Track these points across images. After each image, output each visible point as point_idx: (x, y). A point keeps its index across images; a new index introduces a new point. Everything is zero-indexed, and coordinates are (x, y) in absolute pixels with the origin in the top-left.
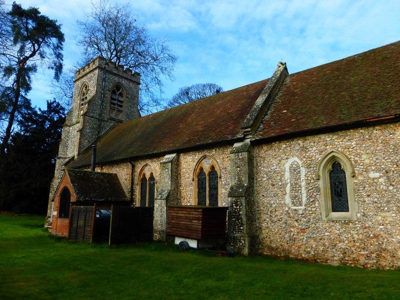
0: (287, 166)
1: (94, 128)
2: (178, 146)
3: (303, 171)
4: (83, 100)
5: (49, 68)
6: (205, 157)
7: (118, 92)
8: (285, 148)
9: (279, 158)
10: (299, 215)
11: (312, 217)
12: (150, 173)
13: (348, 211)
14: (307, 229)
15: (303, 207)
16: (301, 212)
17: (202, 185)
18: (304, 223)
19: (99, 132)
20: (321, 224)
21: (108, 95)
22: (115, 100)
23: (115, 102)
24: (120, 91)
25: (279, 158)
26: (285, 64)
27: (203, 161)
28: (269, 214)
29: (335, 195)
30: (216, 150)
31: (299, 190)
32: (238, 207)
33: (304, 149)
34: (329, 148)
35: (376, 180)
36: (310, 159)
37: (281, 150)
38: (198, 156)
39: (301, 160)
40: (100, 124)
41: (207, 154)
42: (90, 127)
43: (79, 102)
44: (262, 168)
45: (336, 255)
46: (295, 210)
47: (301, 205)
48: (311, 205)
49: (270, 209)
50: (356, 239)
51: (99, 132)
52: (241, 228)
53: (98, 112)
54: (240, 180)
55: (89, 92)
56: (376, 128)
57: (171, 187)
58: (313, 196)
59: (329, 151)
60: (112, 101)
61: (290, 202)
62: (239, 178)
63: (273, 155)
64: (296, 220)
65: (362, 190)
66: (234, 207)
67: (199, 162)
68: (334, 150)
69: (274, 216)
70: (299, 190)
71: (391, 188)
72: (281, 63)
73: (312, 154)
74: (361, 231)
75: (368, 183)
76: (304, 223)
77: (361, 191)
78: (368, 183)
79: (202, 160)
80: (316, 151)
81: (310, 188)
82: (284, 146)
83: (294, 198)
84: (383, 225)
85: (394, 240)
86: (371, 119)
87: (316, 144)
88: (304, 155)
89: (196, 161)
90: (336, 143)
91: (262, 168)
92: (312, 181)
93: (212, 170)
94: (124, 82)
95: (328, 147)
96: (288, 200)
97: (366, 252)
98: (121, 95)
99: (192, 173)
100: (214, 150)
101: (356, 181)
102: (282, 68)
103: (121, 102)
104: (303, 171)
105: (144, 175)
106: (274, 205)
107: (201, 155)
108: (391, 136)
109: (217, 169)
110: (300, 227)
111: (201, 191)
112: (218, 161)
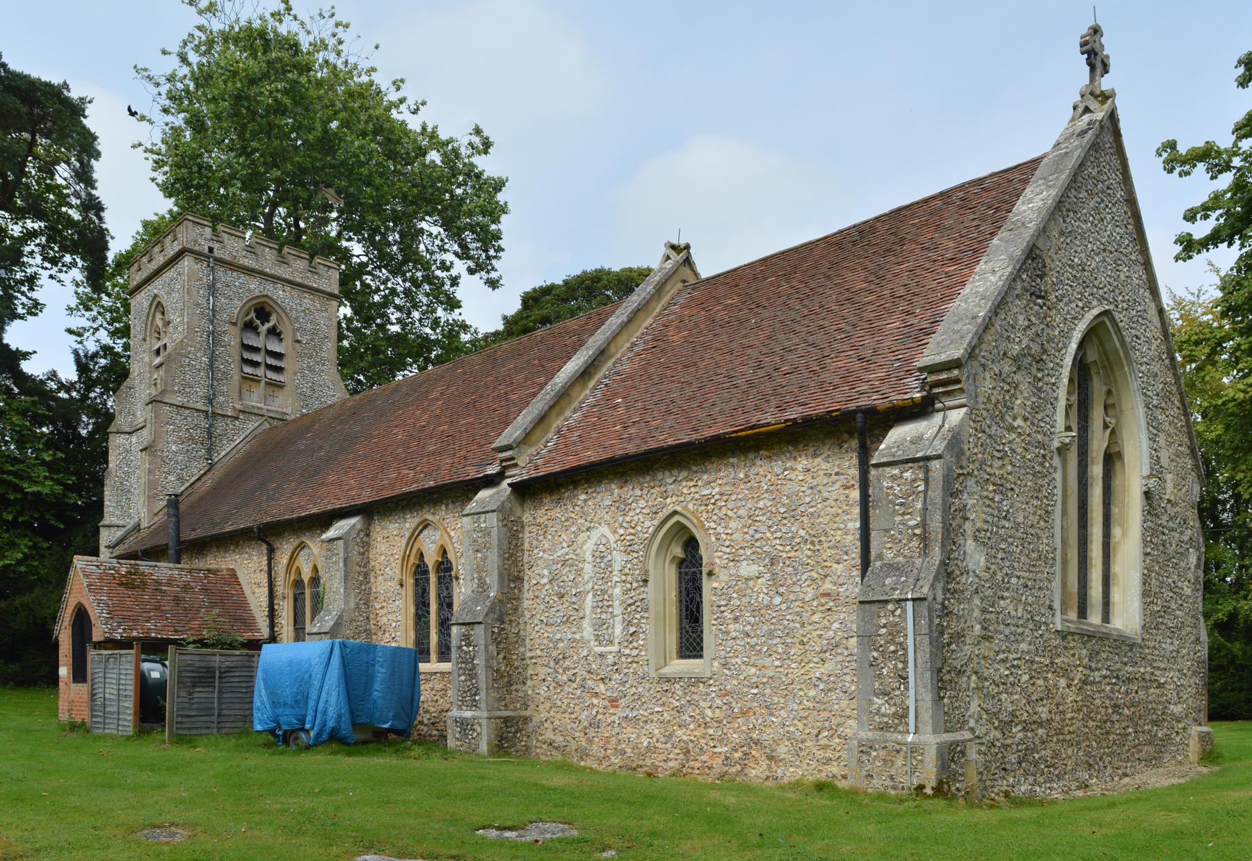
0: (589, 547)
1: (191, 439)
2: (367, 496)
3: (618, 559)
4: (158, 352)
5: (347, 26)
6: (426, 525)
7: (267, 326)
8: (585, 501)
9: (573, 529)
10: (608, 666)
11: (632, 670)
12: (311, 565)
13: (701, 657)
14: (621, 698)
15: (615, 648)
16: (610, 659)
17: (423, 596)
18: (616, 686)
19: (209, 451)
20: (647, 686)
21: (232, 338)
22: (256, 350)
23: (257, 358)
24: (271, 324)
25: (573, 529)
26: (687, 247)
27: (422, 536)
28: (552, 664)
29: (687, 618)
30: (447, 506)
31: (608, 607)
32: (471, 648)
33: (622, 506)
34: (671, 504)
35: (751, 583)
36: (633, 531)
37: (577, 508)
38: (410, 522)
39: (615, 532)
40: (211, 426)
41: (429, 517)
42: (180, 438)
43: (147, 360)
44: (541, 553)
45: (671, 756)
46: (601, 655)
47: (611, 643)
48: (631, 642)
49: (555, 654)
50: (708, 720)
51: (209, 451)
52: (477, 698)
53: (202, 391)
54: (482, 583)
55: (170, 328)
56: (761, 452)
57: (347, 602)
58: (635, 621)
59: (670, 509)
60: (247, 355)
61: (592, 637)
62: (480, 578)
63: (563, 519)
64: (602, 679)
65: (725, 606)
66: (464, 648)
67: (414, 537)
68: (678, 508)
69: (561, 670)
70: (608, 607)
71: (777, 600)
72: (673, 247)
73: (636, 518)
74: (718, 702)
75: (737, 588)
76: (616, 686)
77: (722, 609)
78: (737, 588)
79: (421, 531)
80: (644, 511)
81: (630, 601)
82: (583, 497)
83: (600, 625)
84: (757, 687)
85: (775, 720)
86: (742, 430)
87: (645, 492)
88: (621, 519)
89: (407, 535)
90: (685, 491)
91: (541, 553)
92: (635, 585)
93: (443, 557)
94: (280, 294)
95: (668, 500)
96: (588, 631)
97: (725, 749)
98: (274, 333)
99: (399, 566)
100: (443, 507)
101: (715, 585)
102: (677, 258)
103: (279, 356)
104: (618, 559)
105: (299, 572)
106: (562, 645)
107: (417, 520)
108: (786, 473)
109: (451, 556)
110: (609, 694)
111: (420, 612)
112: (452, 534)
